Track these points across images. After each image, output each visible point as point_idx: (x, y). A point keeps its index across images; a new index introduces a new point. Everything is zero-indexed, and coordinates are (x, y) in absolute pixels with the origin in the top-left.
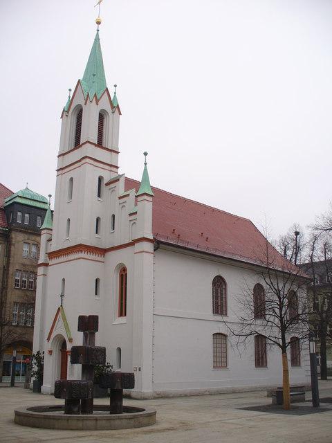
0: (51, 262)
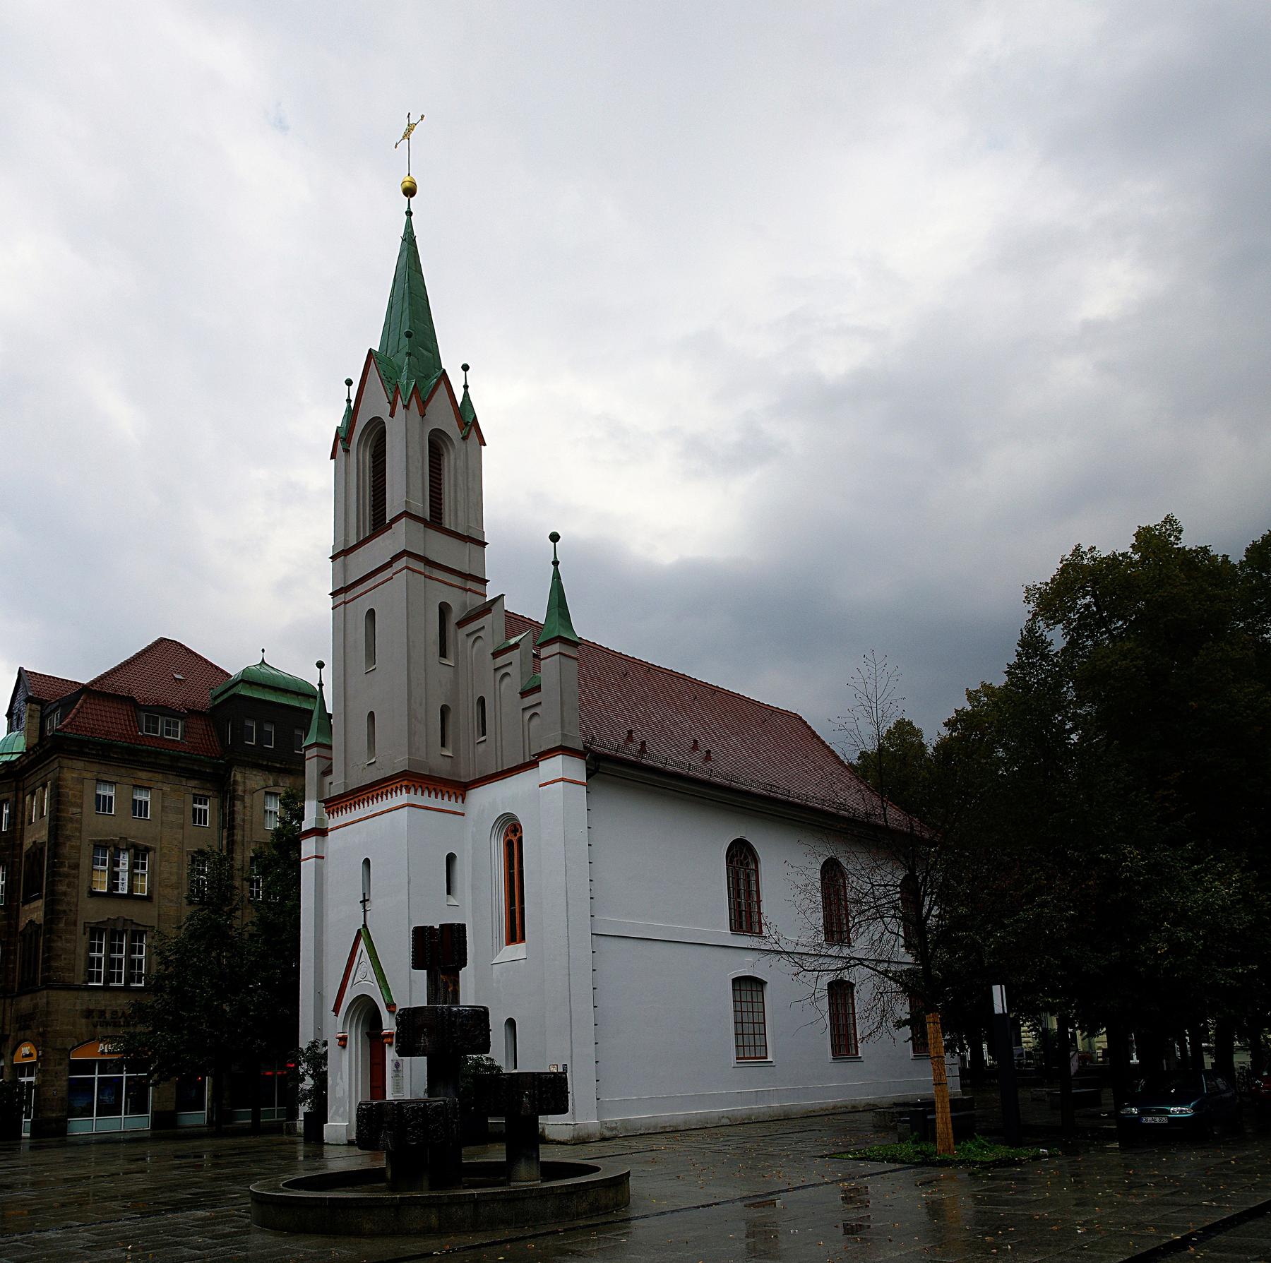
0: (332, 822)
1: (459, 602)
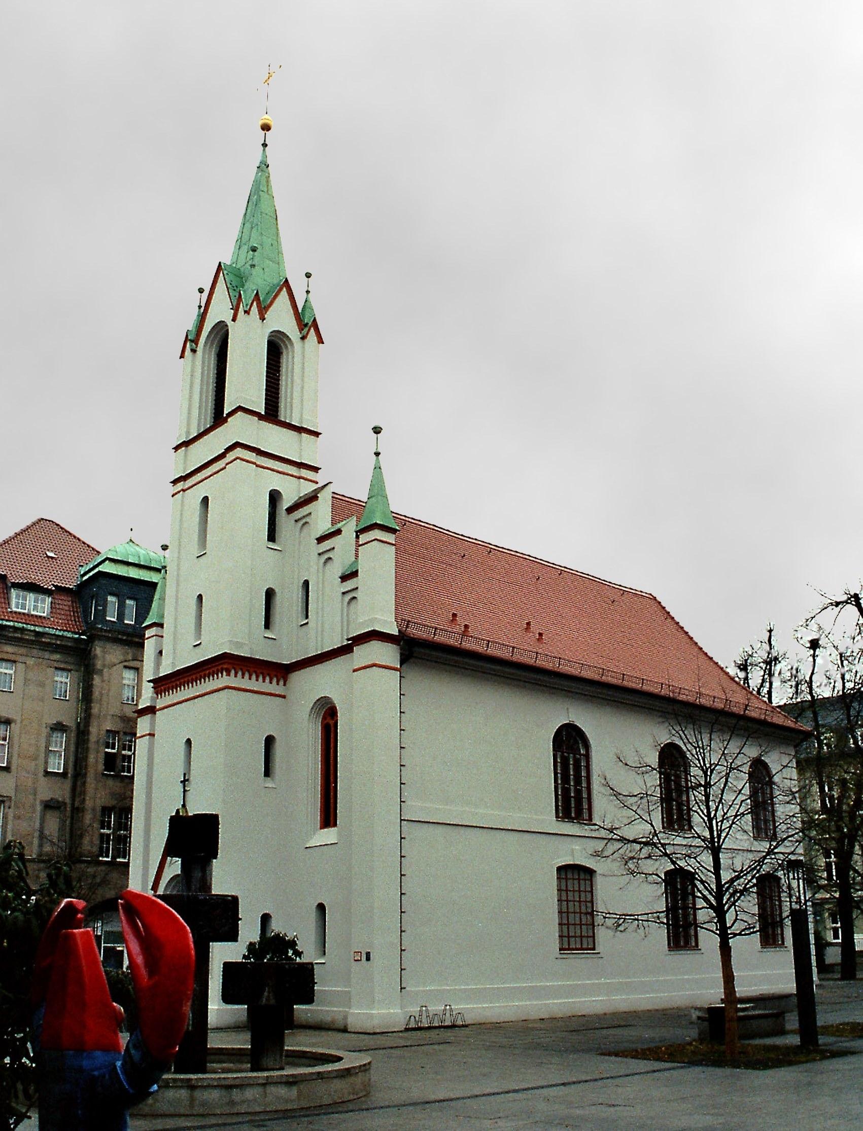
1: (291, 492)
